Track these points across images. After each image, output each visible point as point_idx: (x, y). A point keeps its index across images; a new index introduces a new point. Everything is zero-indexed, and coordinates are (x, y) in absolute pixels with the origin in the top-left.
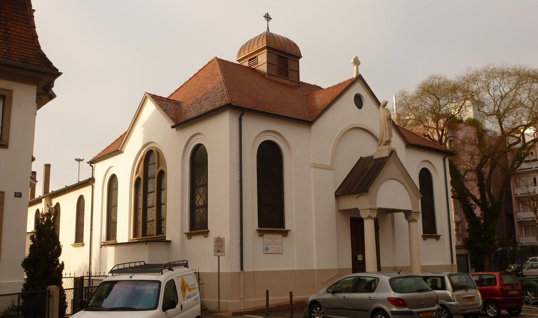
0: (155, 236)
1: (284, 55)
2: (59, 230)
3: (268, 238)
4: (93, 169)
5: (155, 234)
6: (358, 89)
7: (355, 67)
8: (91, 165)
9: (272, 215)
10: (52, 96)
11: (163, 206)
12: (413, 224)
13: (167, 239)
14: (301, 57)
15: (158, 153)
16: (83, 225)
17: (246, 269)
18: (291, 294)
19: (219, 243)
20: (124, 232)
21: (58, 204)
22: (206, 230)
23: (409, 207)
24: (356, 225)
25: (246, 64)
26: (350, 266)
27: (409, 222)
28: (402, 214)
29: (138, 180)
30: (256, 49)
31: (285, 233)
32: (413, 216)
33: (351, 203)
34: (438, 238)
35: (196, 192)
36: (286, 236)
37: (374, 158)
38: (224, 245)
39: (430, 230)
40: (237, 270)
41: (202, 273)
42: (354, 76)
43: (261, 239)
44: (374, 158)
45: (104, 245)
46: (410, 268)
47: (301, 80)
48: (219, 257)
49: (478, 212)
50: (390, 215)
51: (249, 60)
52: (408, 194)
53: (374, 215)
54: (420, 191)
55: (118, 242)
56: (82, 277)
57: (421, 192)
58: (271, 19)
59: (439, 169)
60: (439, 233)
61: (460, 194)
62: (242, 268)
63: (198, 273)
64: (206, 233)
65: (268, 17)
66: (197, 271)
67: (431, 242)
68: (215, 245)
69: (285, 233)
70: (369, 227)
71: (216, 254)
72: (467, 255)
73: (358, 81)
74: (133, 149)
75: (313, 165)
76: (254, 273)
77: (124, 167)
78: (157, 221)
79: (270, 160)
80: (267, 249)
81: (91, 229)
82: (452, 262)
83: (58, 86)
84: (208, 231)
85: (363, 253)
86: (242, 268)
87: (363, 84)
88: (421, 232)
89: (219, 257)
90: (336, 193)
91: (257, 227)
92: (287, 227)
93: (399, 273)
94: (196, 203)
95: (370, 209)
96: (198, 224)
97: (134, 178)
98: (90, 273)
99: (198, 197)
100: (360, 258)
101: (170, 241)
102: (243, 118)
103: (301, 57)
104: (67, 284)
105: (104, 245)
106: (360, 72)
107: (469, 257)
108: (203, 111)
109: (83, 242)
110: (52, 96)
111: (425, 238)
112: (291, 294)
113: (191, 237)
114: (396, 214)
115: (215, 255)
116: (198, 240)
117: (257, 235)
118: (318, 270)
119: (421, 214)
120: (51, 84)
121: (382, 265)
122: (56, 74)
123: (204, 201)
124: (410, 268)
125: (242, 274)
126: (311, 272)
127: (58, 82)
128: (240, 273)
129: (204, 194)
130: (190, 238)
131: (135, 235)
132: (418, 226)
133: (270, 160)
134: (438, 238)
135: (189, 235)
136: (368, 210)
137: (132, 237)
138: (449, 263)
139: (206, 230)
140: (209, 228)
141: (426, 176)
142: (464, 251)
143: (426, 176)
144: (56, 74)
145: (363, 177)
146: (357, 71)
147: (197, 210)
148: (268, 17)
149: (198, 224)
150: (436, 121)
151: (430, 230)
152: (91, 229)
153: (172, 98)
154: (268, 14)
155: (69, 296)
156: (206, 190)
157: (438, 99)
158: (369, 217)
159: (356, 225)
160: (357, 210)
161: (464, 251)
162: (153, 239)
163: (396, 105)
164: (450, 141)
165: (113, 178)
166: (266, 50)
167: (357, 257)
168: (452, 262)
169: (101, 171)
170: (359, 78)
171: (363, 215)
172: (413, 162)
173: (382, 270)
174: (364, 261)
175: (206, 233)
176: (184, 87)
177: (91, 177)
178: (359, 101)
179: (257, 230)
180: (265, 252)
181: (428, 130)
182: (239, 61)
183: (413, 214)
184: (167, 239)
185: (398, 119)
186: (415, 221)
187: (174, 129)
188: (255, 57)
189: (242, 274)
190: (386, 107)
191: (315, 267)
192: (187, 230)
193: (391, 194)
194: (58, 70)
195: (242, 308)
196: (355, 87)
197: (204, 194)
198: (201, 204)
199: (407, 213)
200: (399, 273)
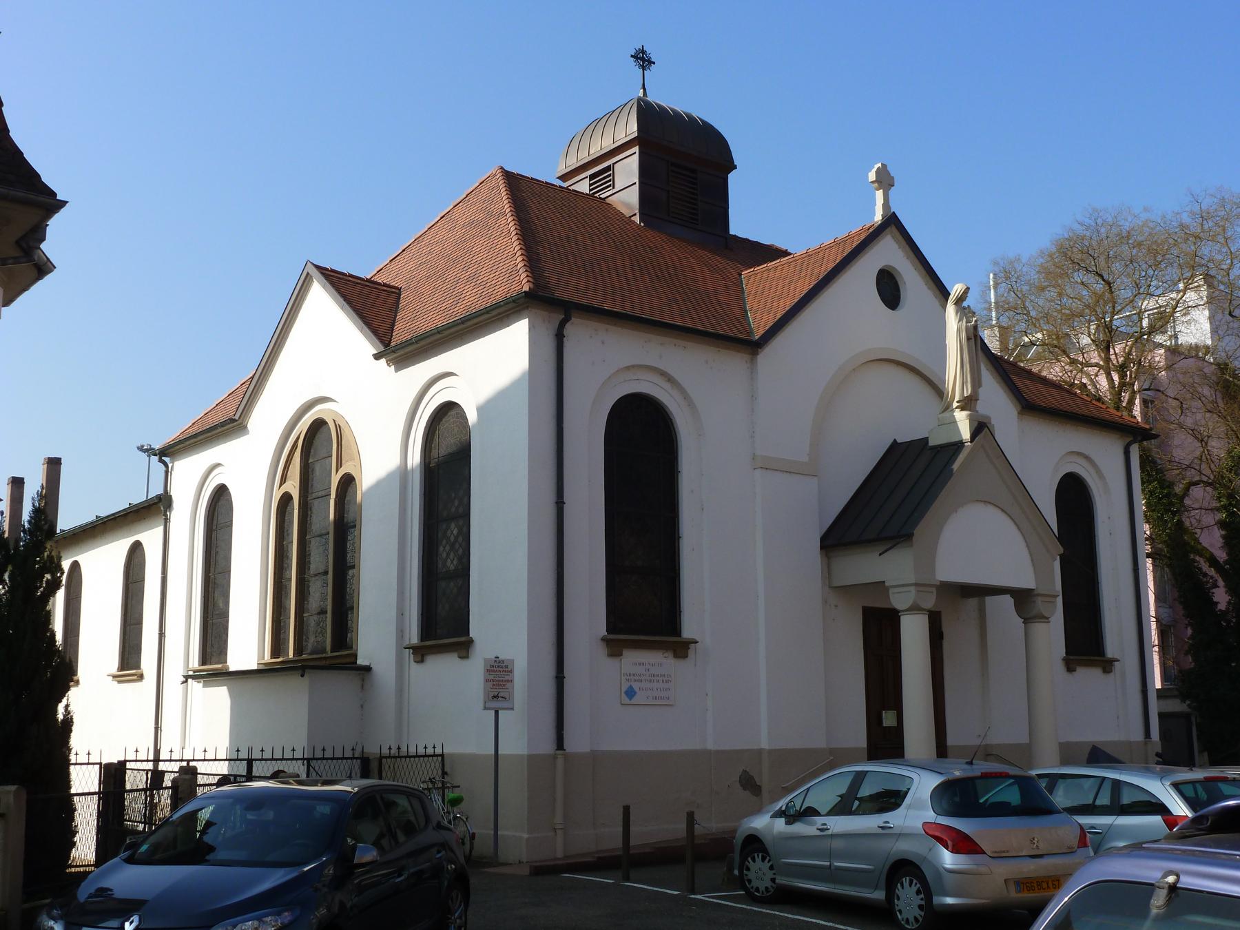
0: (330, 654)
1: (685, 162)
2: (78, 635)
3: (634, 660)
4: (167, 472)
5: (328, 648)
6: (888, 253)
7: (879, 195)
8: (161, 461)
9: (646, 601)
10: (42, 269)
11: (350, 572)
12: (1039, 628)
13: (360, 662)
14: (735, 167)
15: (338, 429)
16: (139, 623)
17: (571, 745)
18: (691, 818)
19: (499, 672)
20: (247, 645)
21: (75, 566)
22: (463, 639)
23: (1025, 579)
24: (880, 630)
25: (584, 187)
26: (862, 743)
27: (1027, 621)
28: (1008, 600)
29: (286, 499)
30: (608, 144)
31: (681, 649)
32: (1040, 605)
33: (867, 567)
34: (1107, 665)
35: (440, 535)
36: (685, 656)
37: (931, 443)
38: (511, 681)
39: (1085, 644)
40: (546, 746)
41: (452, 755)
42: (878, 217)
43: (614, 662)
44: (931, 443)
45: (193, 677)
46: (1026, 752)
47: (732, 232)
48: (497, 713)
49: (1221, 597)
50: (973, 602)
51: (592, 177)
52: (1023, 544)
53: (930, 602)
54: (1058, 539)
55: (231, 669)
56: (122, 764)
57: (1061, 539)
58: (651, 63)
59: (1107, 469)
60: (1111, 651)
61: (1176, 553)
62: (560, 744)
63: (442, 756)
64: (463, 647)
65: (643, 59)
66: (438, 751)
67: (1089, 676)
68: (487, 681)
69: (681, 649)
70: (913, 635)
71: (490, 705)
72: (1185, 716)
73: (888, 230)
74: (271, 419)
75: (755, 457)
76: (596, 758)
77: (248, 470)
78: (333, 613)
79: (642, 446)
80: (631, 693)
81: (162, 635)
82: (1147, 734)
83: (57, 240)
84: (471, 641)
85: (898, 707)
86: (560, 744)
87: (900, 238)
88: (1061, 650)
89: (497, 713)
90: (823, 539)
91: (602, 630)
92: (687, 633)
93: (971, 763)
94: (440, 566)
95: (916, 585)
96: (443, 619)
97: (277, 496)
98: (157, 752)
99: (443, 550)
100: (889, 719)
101: (368, 669)
102: (569, 330)
103: (735, 167)
104: (84, 780)
105: (190, 677)
106: (894, 208)
107: (1193, 719)
108: (460, 311)
109: (139, 667)
110: (42, 269)
111: (1070, 666)
112: (691, 818)
113: (423, 656)
114: (990, 600)
115: (485, 708)
116: (443, 667)
117: (602, 650)
118: (771, 752)
119: (1060, 600)
120: (38, 233)
121: (951, 741)
122: (50, 203)
123: (460, 559)
124: (1026, 752)
125: (560, 762)
126: (707, 753)
127: (56, 226)
128: (555, 757)
129: (460, 539)
130: (422, 661)
131: (278, 646)
132: (1052, 634)
133: (642, 446)
134: (1107, 665)
135: (420, 653)
136: (912, 589)
137: (267, 657)
138: (1137, 735)
139: (463, 639)
140: (473, 633)
141: (1074, 497)
142: (1175, 706)
143: (1074, 497)
144: (50, 203)
145: (898, 492)
146: (886, 205)
147: (443, 584)
148: (643, 59)
149: (443, 619)
150: (1105, 347)
151: (1085, 644)
152: (162, 635)
153: (379, 279)
154: (643, 52)
155: (86, 817)
156: (465, 529)
157: (1109, 284)
158: (915, 609)
159: (880, 630)
160: (880, 587)
161: (1175, 706)
162: (323, 663)
163: (997, 308)
164: (1145, 403)
165: (221, 497)
166: (636, 149)
167: (880, 719)
168: (1147, 734)
169: (187, 479)
170: (892, 221)
171: (899, 601)
172: (1043, 456)
173: (950, 752)
174: (898, 731)
175: (463, 647)
176: (414, 249)
177: (161, 491)
178: (889, 288)
179: (603, 639)
180: (626, 700)
181: (1081, 371)
182: (564, 178)
183: (1039, 600)
184: (360, 662)
185: (1004, 347)
186: (1044, 619)
187: (383, 361)
188: (608, 169)
189: (560, 762)
190: (965, 304)
191: (765, 744)
192: (414, 637)
193: (981, 543)
194: (55, 195)
195: (560, 854)
196: (889, 259)
197: (460, 539)
198: (452, 567)
199: (1023, 598)
200: (971, 763)
